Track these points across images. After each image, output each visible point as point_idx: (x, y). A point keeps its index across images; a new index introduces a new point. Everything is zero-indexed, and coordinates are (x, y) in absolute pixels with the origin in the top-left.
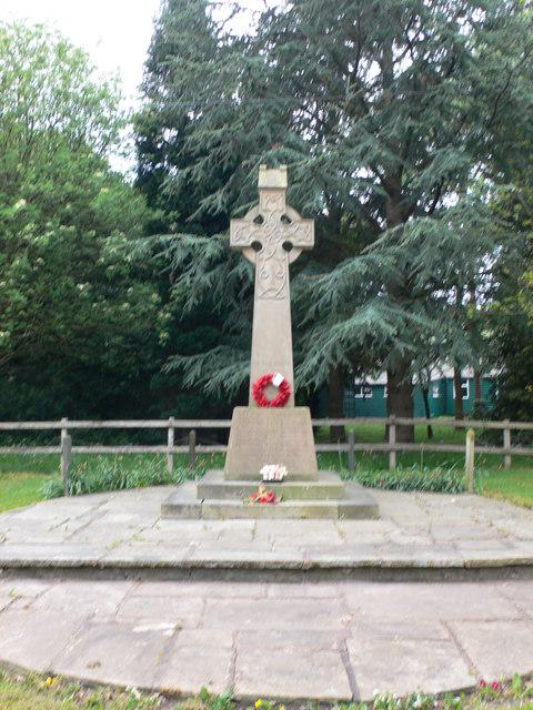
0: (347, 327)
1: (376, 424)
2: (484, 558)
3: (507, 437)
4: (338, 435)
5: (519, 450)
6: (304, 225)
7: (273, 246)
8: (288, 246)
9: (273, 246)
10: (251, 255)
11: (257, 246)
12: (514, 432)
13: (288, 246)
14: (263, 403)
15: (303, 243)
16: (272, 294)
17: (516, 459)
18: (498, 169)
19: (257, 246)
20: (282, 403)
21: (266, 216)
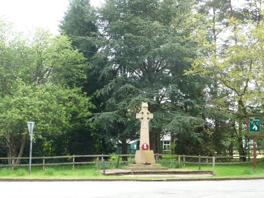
0: (57, 177)
1: (168, 156)
2: (144, 175)
3: (200, 160)
4: (160, 157)
5: (187, 162)
6: (151, 114)
7: (145, 118)
8: (148, 118)
9: (145, 118)
10: (141, 120)
11: (142, 118)
12: (186, 158)
13: (148, 118)
14: (143, 149)
15: (151, 118)
16: (145, 128)
17: (76, 165)
18: (132, 138)
19: (148, 113)
20: (147, 149)
21: (144, 112)
